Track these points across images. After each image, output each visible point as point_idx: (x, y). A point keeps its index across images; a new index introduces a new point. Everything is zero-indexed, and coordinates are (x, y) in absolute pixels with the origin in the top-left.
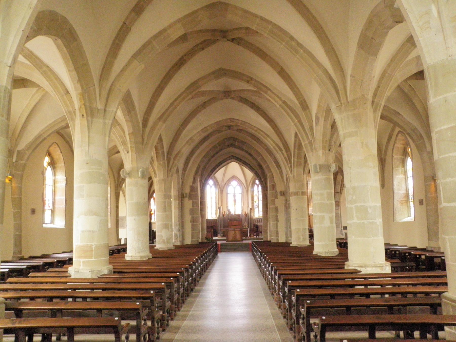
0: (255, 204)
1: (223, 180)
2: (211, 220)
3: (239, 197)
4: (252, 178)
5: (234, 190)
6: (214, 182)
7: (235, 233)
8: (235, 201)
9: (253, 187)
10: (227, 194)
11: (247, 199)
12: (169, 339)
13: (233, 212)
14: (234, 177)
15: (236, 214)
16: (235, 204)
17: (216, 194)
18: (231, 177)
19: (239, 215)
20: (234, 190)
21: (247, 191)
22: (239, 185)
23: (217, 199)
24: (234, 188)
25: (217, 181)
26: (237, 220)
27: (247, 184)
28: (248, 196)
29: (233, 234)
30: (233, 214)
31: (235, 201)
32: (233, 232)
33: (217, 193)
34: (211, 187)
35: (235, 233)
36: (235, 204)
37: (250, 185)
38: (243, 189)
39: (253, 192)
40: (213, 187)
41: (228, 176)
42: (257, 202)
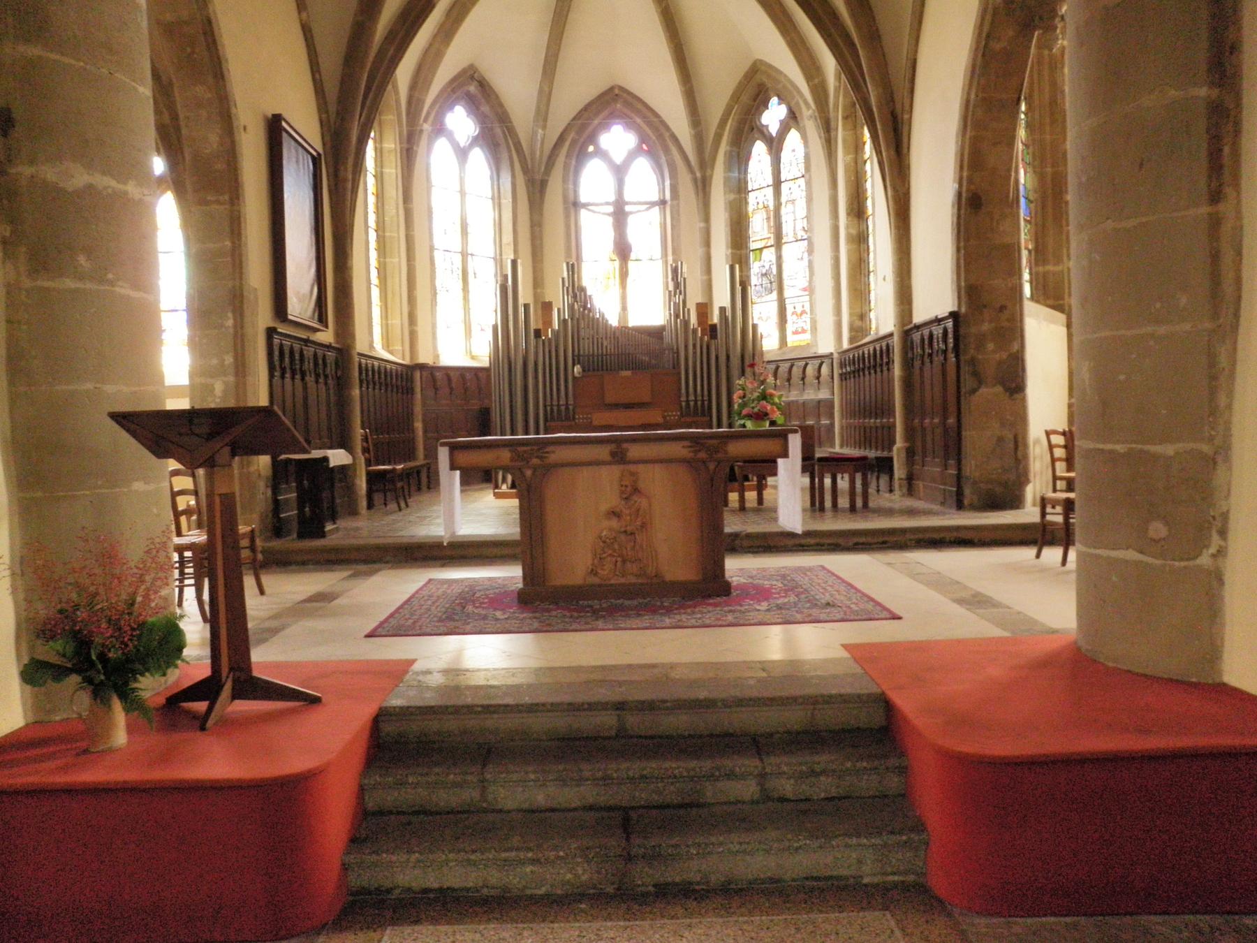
0: (755, 268)
1: (542, 114)
2: (462, 371)
3: (646, 231)
4: (736, 97)
5: (618, 179)
6: (481, 119)
7: (631, 491)
8: (623, 251)
9: (740, 158)
10: (573, 205)
11: (697, 237)
12: (491, 687)
13: (606, 307)
14: (615, 102)
15: (632, 322)
16: (624, 275)
17: (498, 206)
18: (594, 92)
19: (656, 333)
20: (618, 179)
21: (703, 187)
22: (651, 154)
23: (508, 237)
24: (620, 172)
25: (503, 117)
26: (636, 366)
27: (699, 139)
28: (707, 219)
29: (610, 498)
30: (613, 321)
31: (623, 251)
32: (609, 476)
33: (507, 201)
34: (462, 153)
35: (631, 491)
36: (624, 275)
37: (724, 147)
38: (673, 176)
39: (740, 189)
40: (478, 157)
41: (573, 94)
42: (769, 255)
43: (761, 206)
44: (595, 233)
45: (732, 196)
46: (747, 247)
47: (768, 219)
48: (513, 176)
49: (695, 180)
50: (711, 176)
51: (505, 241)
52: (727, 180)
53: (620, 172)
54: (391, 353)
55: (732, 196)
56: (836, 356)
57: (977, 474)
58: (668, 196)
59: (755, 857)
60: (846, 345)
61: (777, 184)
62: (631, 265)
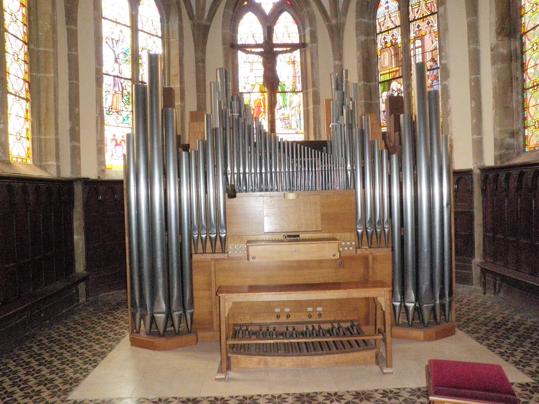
8: (271, 83)
21: (336, 33)
28: (313, 80)
39: (369, 31)
43: (389, 45)
44: (250, 72)
45: (363, 38)
46: (376, 80)
47: (396, 54)
48: (181, 19)
49: (331, 28)
50: (344, 24)
51: (172, 73)
52: (358, 26)
53: (269, 23)
54: (43, 168)
55: (363, 38)
56: (477, 172)
57: (14, 159)
58: (308, 40)
59: (213, 277)
60: (489, 161)
61: (406, 23)
62: (279, 97)
